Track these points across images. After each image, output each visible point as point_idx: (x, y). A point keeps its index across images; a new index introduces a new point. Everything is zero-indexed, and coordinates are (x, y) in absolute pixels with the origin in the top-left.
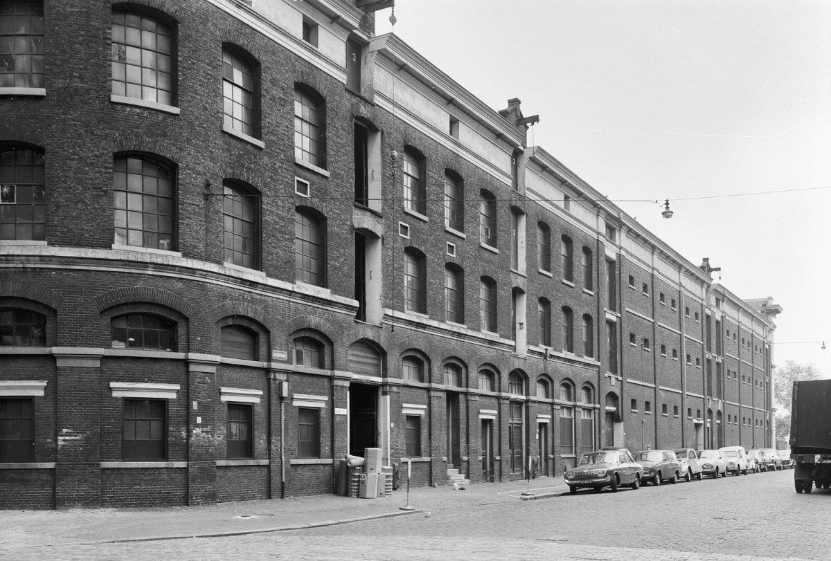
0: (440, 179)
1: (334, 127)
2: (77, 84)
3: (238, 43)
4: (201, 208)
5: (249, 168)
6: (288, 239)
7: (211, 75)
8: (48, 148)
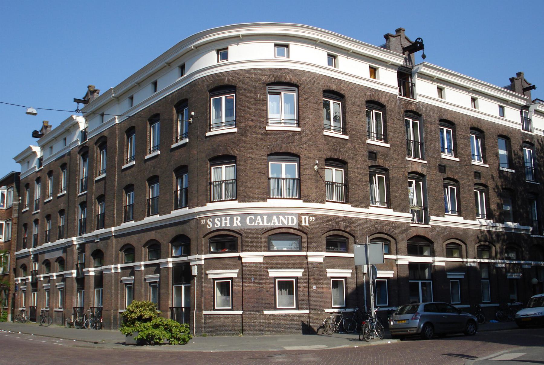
0: (467, 135)
1: (392, 119)
2: (251, 123)
3: (332, 89)
4: (313, 176)
5: (340, 151)
6: (364, 184)
7: (317, 108)
8: (238, 156)
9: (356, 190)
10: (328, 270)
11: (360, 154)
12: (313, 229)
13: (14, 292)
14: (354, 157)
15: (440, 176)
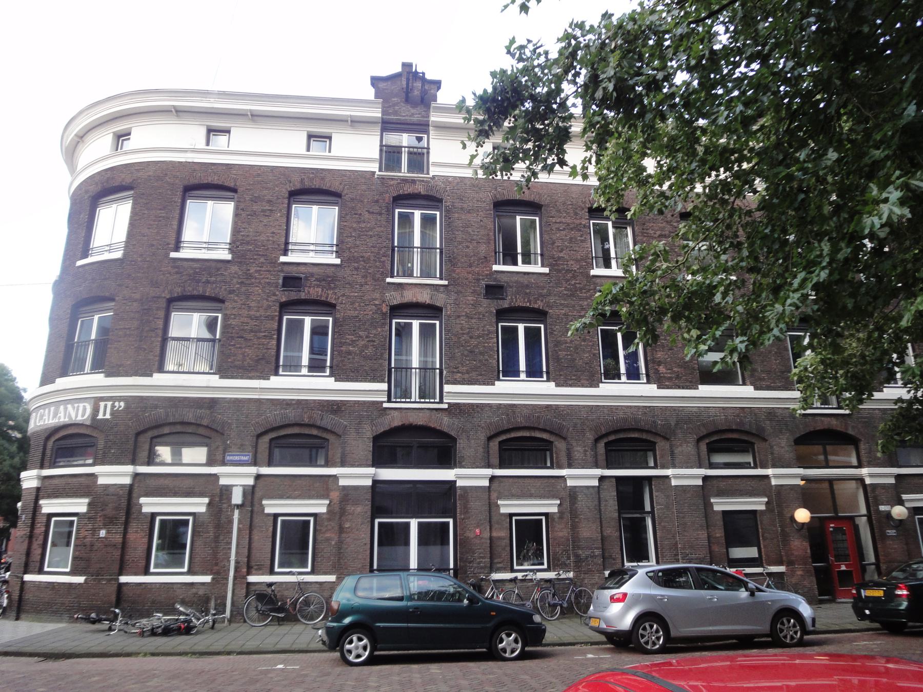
9: (240, 348)
10: (143, 500)
11: (260, 283)
12: (116, 425)
13: (12, 530)
14: (243, 289)
15: (489, 306)
